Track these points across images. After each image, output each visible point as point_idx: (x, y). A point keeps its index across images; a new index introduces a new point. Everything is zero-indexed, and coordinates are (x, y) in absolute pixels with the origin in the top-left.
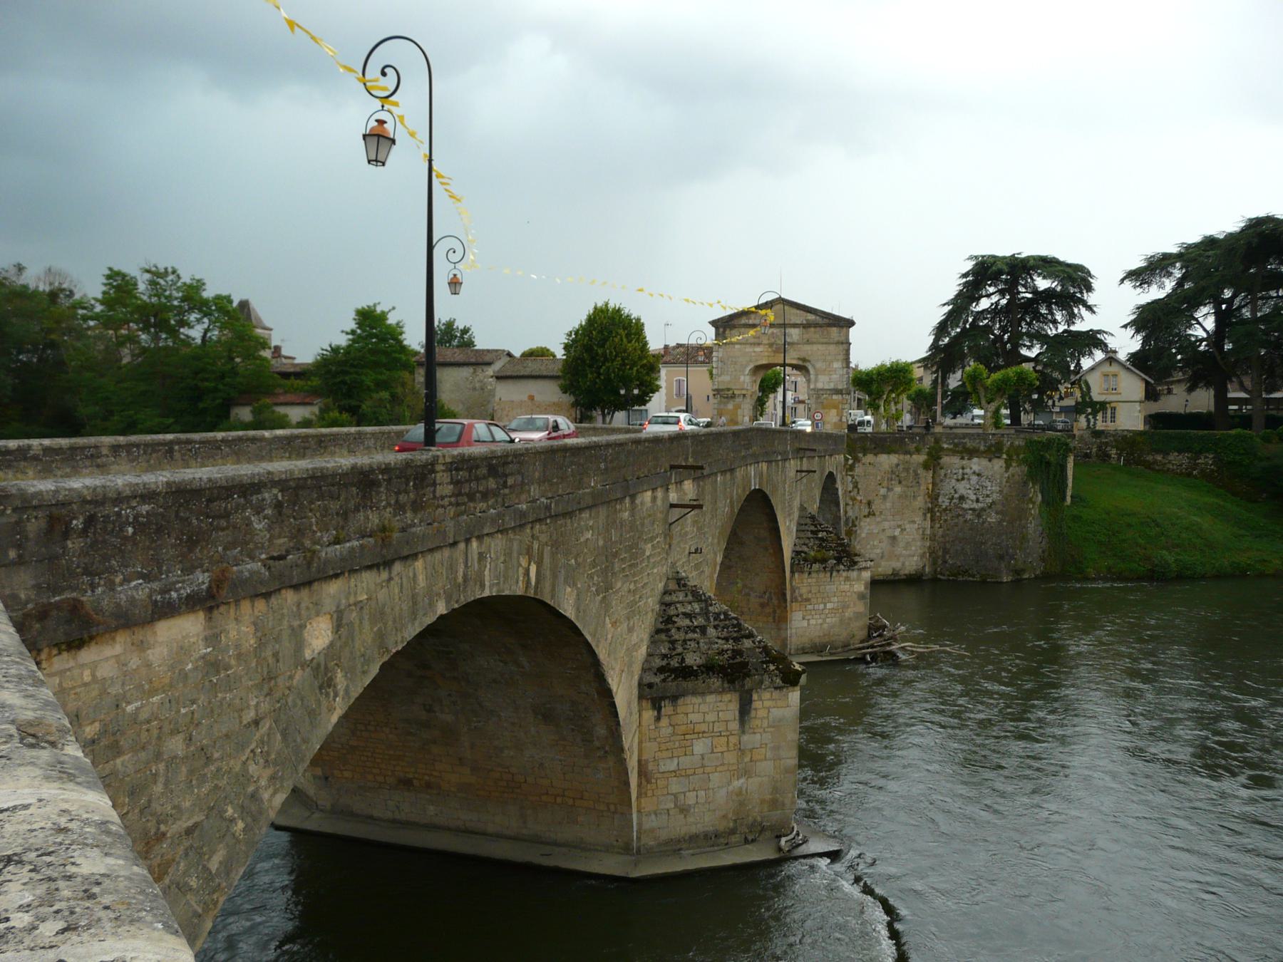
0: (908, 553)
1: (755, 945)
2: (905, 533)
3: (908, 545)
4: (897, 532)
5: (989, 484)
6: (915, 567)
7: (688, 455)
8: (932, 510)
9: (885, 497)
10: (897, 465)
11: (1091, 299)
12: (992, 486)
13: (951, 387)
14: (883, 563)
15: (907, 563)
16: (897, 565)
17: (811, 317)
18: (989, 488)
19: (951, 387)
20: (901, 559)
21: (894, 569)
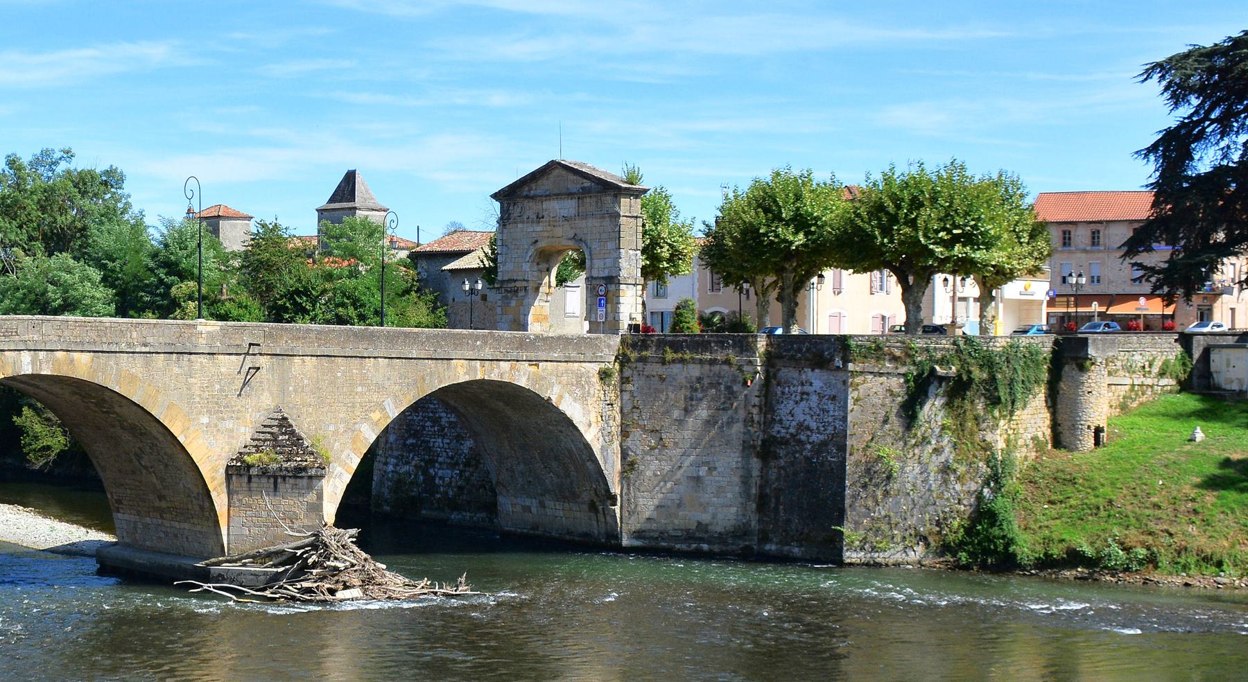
0: (721, 501)
1: (384, 493)
2: (715, 473)
3: (720, 491)
4: (703, 471)
5: (831, 407)
6: (733, 522)
7: (1064, 334)
8: (766, 449)
9: (680, 422)
10: (699, 379)
11: (856, 185)
12: (834, 411)
13: (266, 394)
14: (680, 514)
15: (720, 516)
16: (705, 518)
17: (587, 184)
18: (831, 413)
19: (266, 394)
20: (711, 509)
21: (699, 523)
